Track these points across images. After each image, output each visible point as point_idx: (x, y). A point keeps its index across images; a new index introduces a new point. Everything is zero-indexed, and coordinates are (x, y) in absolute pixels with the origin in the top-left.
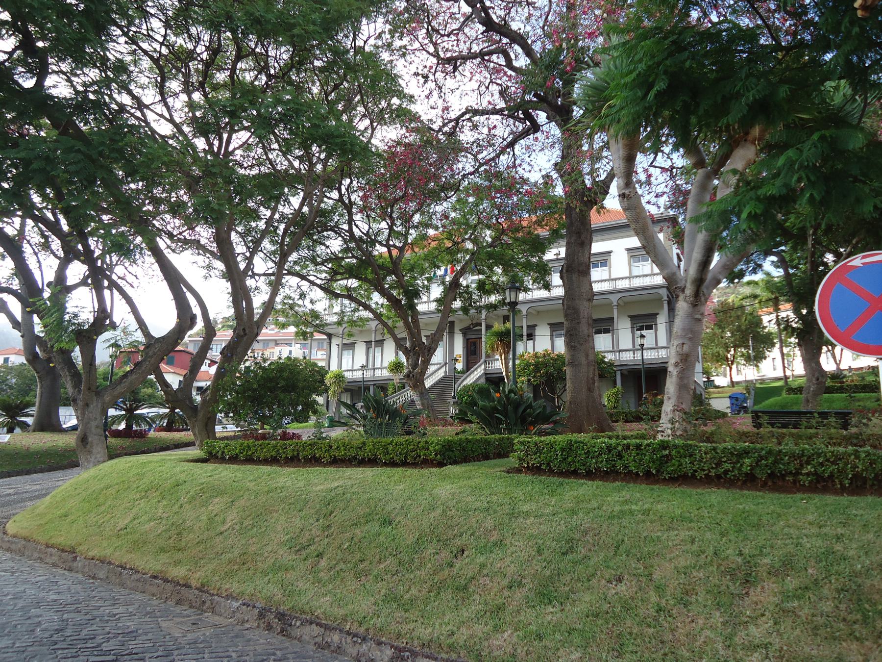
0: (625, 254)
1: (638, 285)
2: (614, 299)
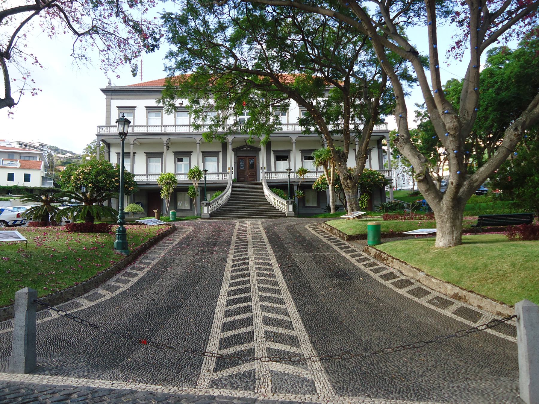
2: (294, 138)
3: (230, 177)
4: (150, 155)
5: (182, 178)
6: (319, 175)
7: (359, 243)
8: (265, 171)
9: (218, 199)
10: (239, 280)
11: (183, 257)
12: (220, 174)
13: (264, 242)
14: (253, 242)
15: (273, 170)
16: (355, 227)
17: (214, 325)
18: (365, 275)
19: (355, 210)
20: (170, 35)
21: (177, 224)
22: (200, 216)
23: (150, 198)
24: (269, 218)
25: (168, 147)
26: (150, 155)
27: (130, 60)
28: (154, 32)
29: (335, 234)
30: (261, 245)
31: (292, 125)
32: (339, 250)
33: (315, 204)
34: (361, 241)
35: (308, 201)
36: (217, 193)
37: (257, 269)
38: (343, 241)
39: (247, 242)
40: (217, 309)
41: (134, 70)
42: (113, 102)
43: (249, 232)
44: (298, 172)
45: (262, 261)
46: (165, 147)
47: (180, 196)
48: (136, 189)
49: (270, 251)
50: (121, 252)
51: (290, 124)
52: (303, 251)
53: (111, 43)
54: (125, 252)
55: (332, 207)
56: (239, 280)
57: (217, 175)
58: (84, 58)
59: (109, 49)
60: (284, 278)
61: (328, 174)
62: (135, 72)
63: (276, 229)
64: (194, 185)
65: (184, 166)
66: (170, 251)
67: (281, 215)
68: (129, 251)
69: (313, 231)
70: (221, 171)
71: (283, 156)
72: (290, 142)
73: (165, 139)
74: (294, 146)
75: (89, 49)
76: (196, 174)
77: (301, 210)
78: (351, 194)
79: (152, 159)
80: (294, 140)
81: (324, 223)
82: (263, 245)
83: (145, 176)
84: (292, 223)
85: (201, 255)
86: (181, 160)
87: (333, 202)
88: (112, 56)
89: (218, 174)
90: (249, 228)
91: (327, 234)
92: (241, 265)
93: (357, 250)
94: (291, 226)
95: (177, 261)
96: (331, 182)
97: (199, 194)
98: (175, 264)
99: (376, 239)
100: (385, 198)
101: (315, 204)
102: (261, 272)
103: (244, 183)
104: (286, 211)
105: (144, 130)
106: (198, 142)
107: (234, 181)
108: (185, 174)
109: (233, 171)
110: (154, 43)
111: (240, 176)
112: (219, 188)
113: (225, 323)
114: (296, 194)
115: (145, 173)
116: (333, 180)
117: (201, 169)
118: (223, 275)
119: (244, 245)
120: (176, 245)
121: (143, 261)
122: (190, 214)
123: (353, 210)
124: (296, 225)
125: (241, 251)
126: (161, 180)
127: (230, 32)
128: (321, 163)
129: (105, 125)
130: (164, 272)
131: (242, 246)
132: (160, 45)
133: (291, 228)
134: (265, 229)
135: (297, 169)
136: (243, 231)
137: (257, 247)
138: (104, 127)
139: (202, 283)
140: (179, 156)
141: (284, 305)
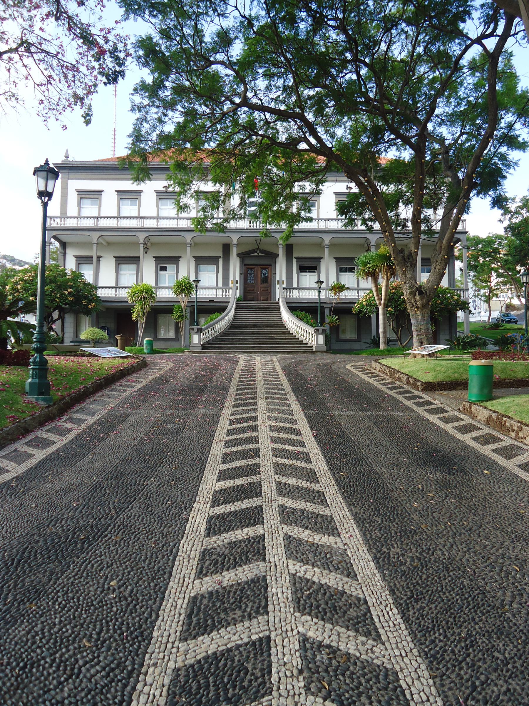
0: (115, 196)
1: (165, 226)
2: (327, 239)
3: (233, 294)
4: (121, 260)
5: (165, 294)
6: (362, 293)
7: (448, 396)
8: (284, 286)
9: (214, 324)
10: (238, 464)
11: (143, 412)
12: (220, 288)
13: (284, 390)
14: (266, 388)
15: (295, 285)
16: (433, 369)
17: (167, 605)
18: (490, 464)
19: (425, 343)
20: (141, 53)
21: (149, 358)
22: (188, 347)
23: (118, 320)
24: (289, 353)
25: (146, 249)
26: (121, 260)
27: (82, 99)
28: (116, 49)
29: (399, 379)
30: (278, 394)
31: (325, 220)
32: (415, 408)
33: (354, 336)
34: (448, 392)
35: (344, 332)
36: (213, 316)
37: (272, 429)
38: (416, 393)
39: (256, 388)
40: (185, 545)
41: (88, 115)
42: (70, 182)
43: (259, 372)
44: (333, 288)
45: (282, 424)
46: (142, 249)
47: (161, 319)
48: (99, 307)
49: (295, 406)
50: (37, 399)
51: (322, 219)
52: (352, 406)
53: (53, 73)
54: (44, 400)
55: (382, 340)
56: (238, 464)
57: (214, 291)
58: (13, 99)
59: (49, 82)
60: (328, 463)
61: (379, 290)
62: (88, 118)
63: (301, 369)
64: (182, 303)
65: (169, 277)
66: (125, 400)
67: (307, 349)
68: (51, 399)
69: (360, 374)
70: (220, 284)
71: (309, 266)
72: (320, 246)
73: (142, 237)
74: (327, 251)
75: (22, 83)
76: (185, 287)
77: (334, 343)
78: (420, 317)
79: (123, 266)
80: (327, 242)
81: (376, 361)
82: (282, 394)
83: (114, 290)
84: (326, 362)
85: (177, 408)
86: (164, 269)
87: (384, 332)
88: (53, 93)
89: (216, 288)
90: (258, 366)
91: (385, 379)
92: (246, 425)
93: (446, 408)
94: (324, 365)
95: (131, 418)
96: (382, 302)
97: (188, 317)
98: (127, 424)
99: (486, 391)
100: (456, 332)
101: (354, 336)
102: (281, 447)
103: (254, 302)
104: (314, 344)
105: (112, 223)
106: (189, 241)
107: (238, 299)
108: (169, 288)
109: (238, 285)
110: (118, 69)
111: (248, 292)
112: (216, 308)
113: (195, 597)
114: (327, 320)
115: (114, 285)
116: (385, 300)
117: (192, 278)
118: (209, 452)
119: (251, 393)
120: (138, 390)
121: (75, 416)
122: (176, 345)
123: (421, 344)
124: (332, 363)
125: (245, 405)
126: (133, 294)
127: (237, 50)
128: (367, 274)
129: (58, 214)
130: (103, 439)
131: (247, 398)
132: (127, 72)
133: (325, 369)
134: (284, 368)
135: (331, 283)
136: (250, 371)
137: (272, 398)
138: (57, 217)
139: (165, 469)
140: (162, 263)
141: (338, 540)
